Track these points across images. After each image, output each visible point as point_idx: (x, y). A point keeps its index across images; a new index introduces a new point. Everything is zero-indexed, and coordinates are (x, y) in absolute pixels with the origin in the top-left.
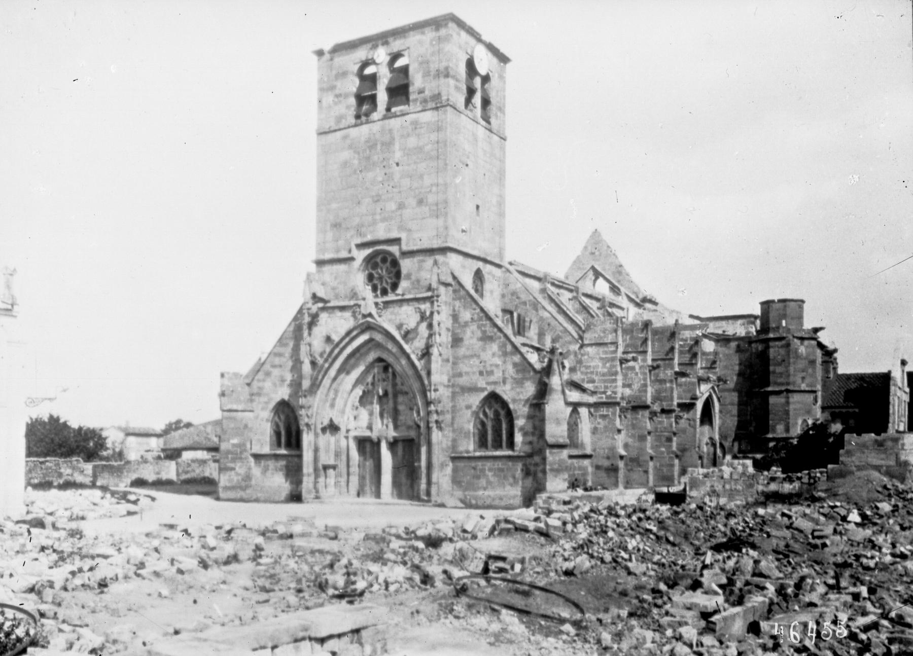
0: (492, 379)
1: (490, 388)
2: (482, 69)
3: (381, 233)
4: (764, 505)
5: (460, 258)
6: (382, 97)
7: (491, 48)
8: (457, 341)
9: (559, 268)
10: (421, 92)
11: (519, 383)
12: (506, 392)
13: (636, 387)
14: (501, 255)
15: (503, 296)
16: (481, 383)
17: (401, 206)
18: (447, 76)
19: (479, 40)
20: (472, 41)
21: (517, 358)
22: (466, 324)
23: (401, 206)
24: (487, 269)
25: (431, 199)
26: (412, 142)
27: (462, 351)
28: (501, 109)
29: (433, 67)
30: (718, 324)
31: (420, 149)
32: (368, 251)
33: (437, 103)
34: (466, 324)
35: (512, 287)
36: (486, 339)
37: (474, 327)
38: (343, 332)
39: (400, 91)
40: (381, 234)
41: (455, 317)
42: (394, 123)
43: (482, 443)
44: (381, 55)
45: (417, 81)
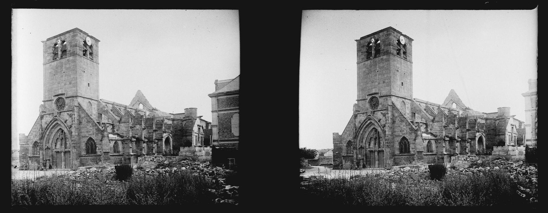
0: (90, 133)
1: (403, 136)
2: (89, 43)
3: (60, 92)
4: (472, 167)
5: (396, 98)
6: (60, 53)
7: (91, 37)
8: (80, 123)
9: (127, 102)
10: (70, 51)
11: (97, 134)
12: (94, 137)
13: (452, 134)
14: (98, 97)
15: (98, 109)
16: (401, 134)
17: (379, 83)
18: (76, 46)
19: (88, 36)
20: (85, 36)
21: (410, 127)
22: (396, 117)
23: (379, 83)
24: (92, 102)
25: (386, 81)
26: (68, 66)
27: (82, 126)
28: (97, 55)
29: (73, 44)
30: (491, 115)
31: (383, 67)
32: (57, 97)
33: (74, 54)
34: (396, 117)
35: (414, 106)
36: (88, 122)
37: (85, 119)
38: (363, 120)
39: (64, 51)
40: (60, 92)
41: (79, 116)
42: (63, 60)
43: (88, 152)
44: (59, 42)
45: (69, 48)
